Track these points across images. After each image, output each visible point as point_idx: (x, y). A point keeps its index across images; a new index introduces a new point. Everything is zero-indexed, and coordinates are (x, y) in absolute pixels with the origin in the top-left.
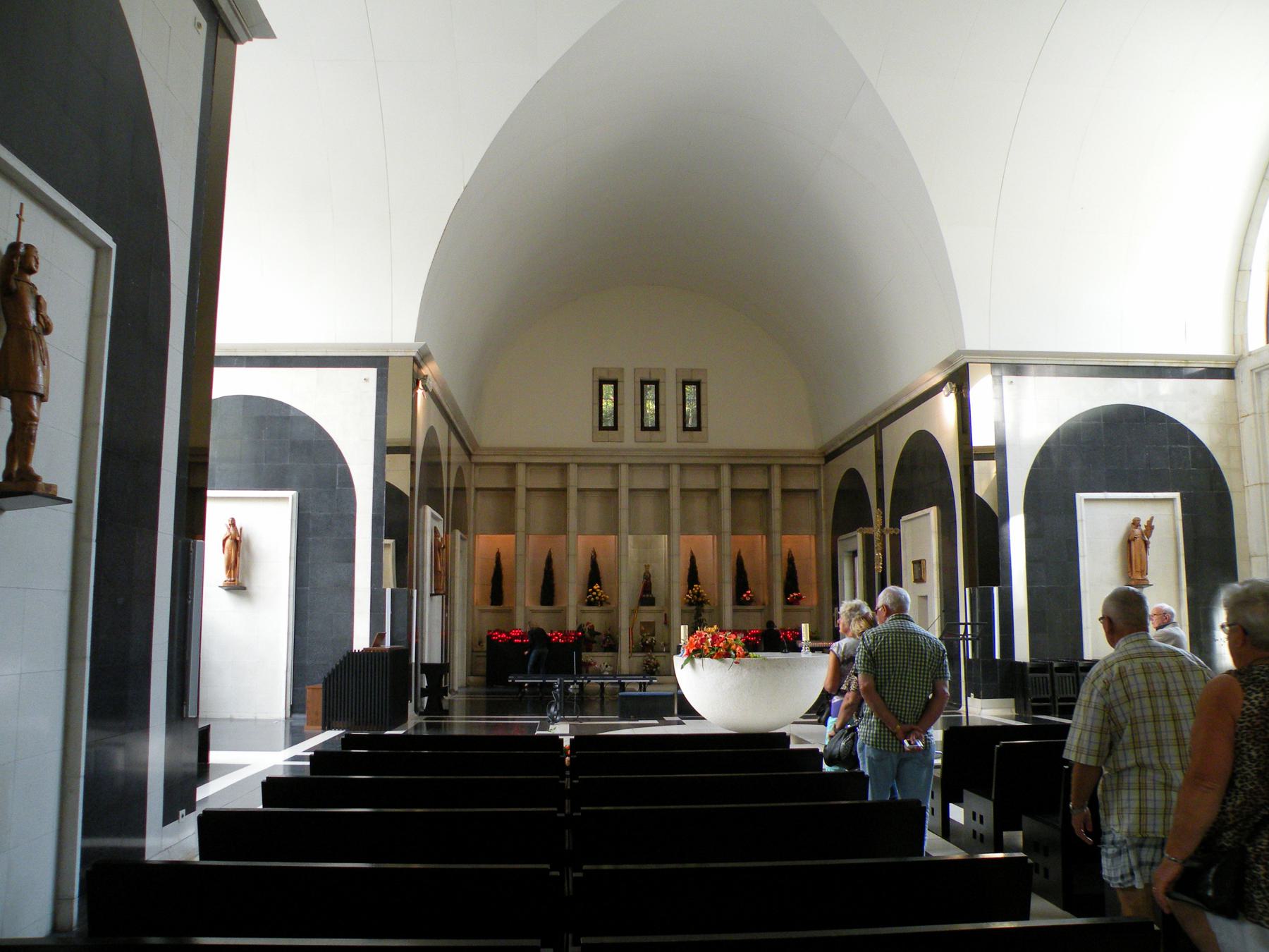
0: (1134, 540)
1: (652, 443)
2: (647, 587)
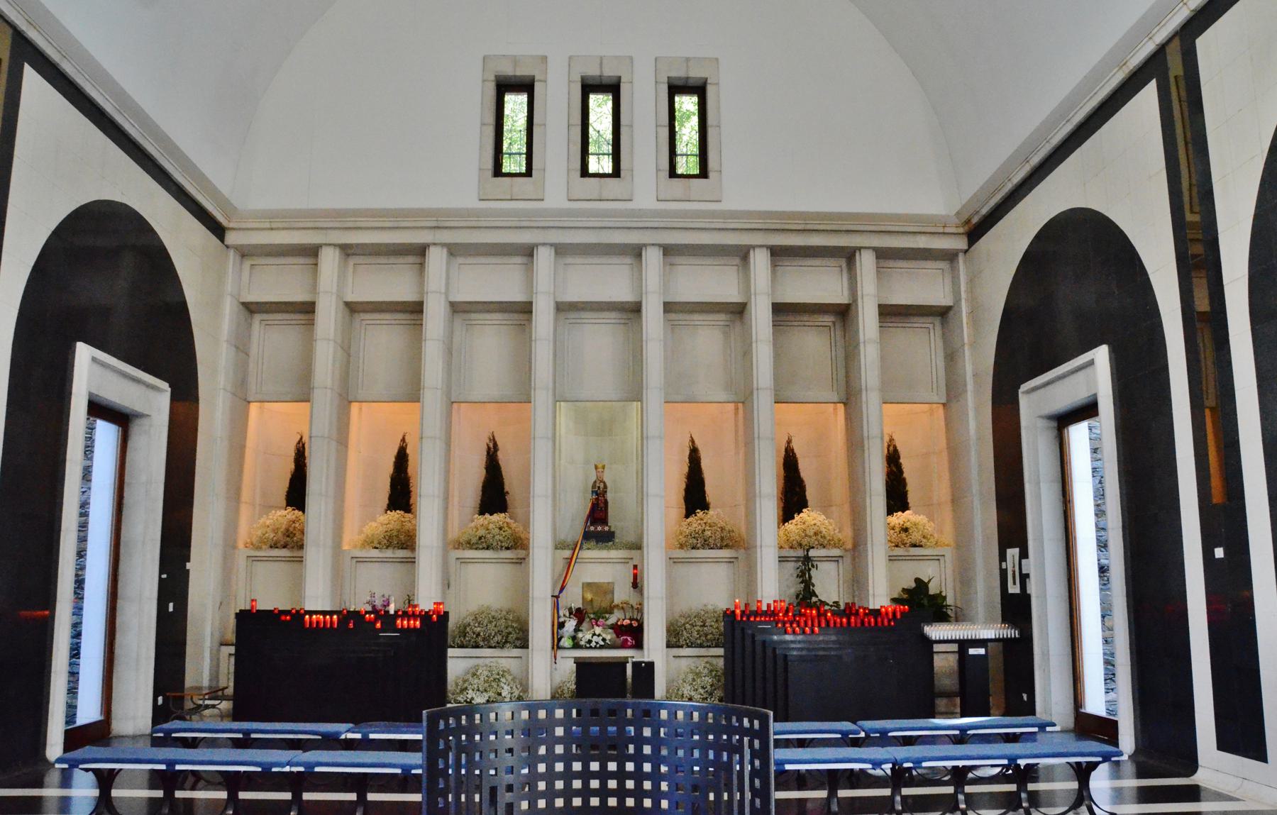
2: (598, 512)
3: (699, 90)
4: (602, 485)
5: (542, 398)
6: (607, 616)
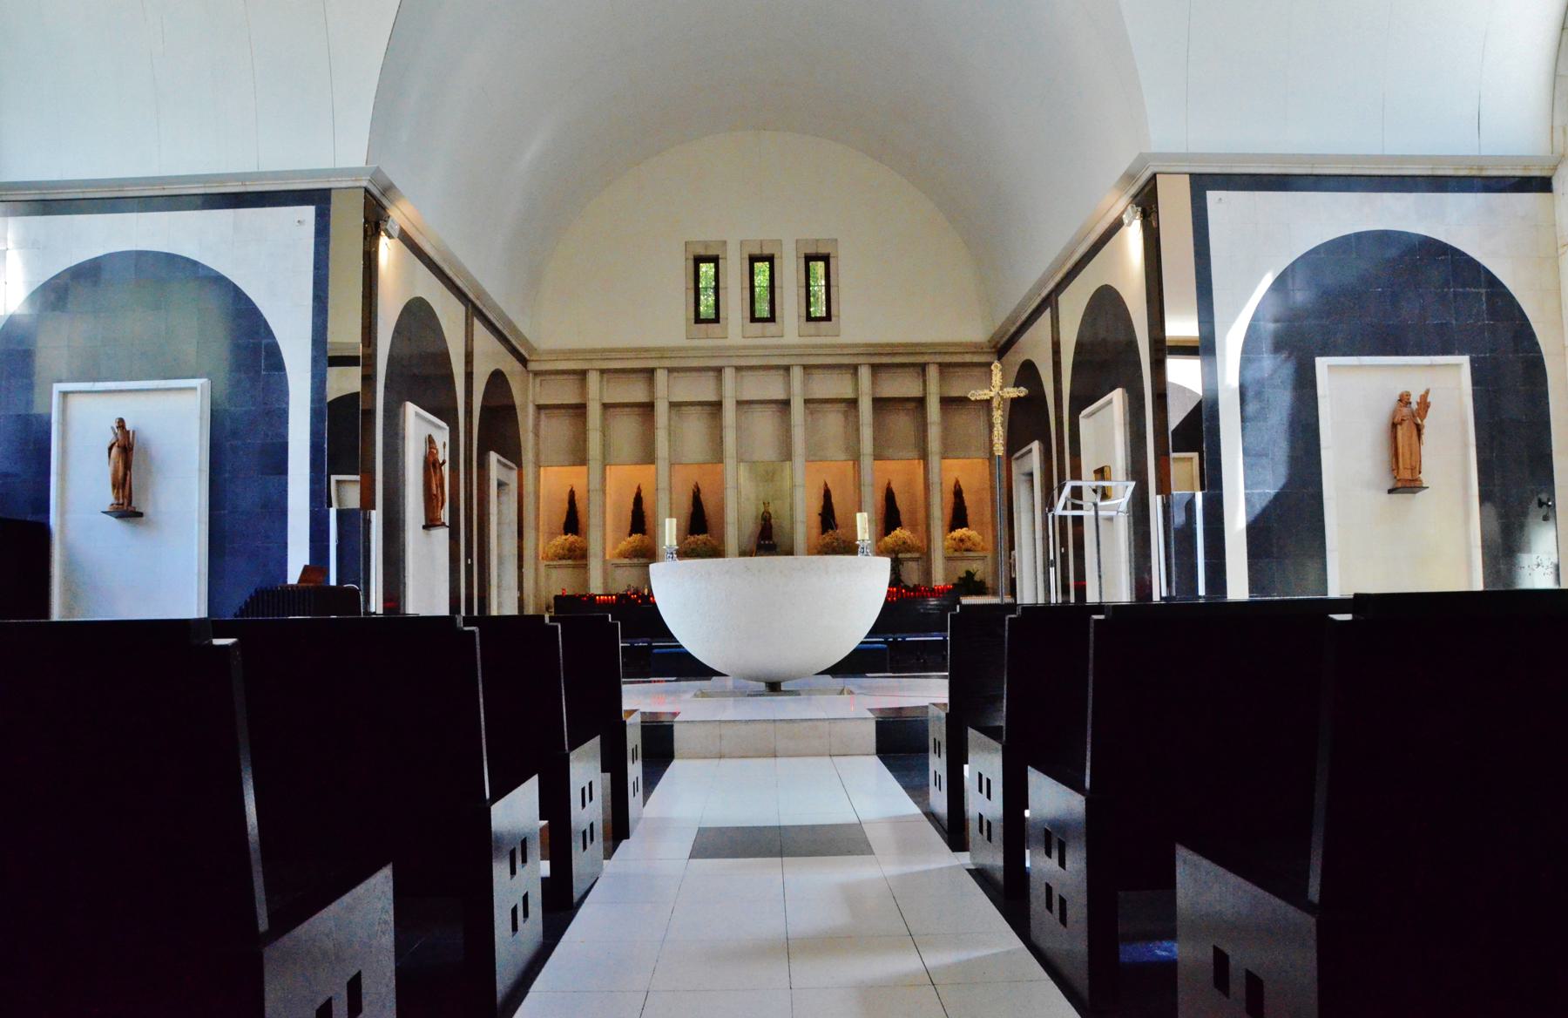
0: (1401, 424)
3: (826, 259)
4: (768, 515)
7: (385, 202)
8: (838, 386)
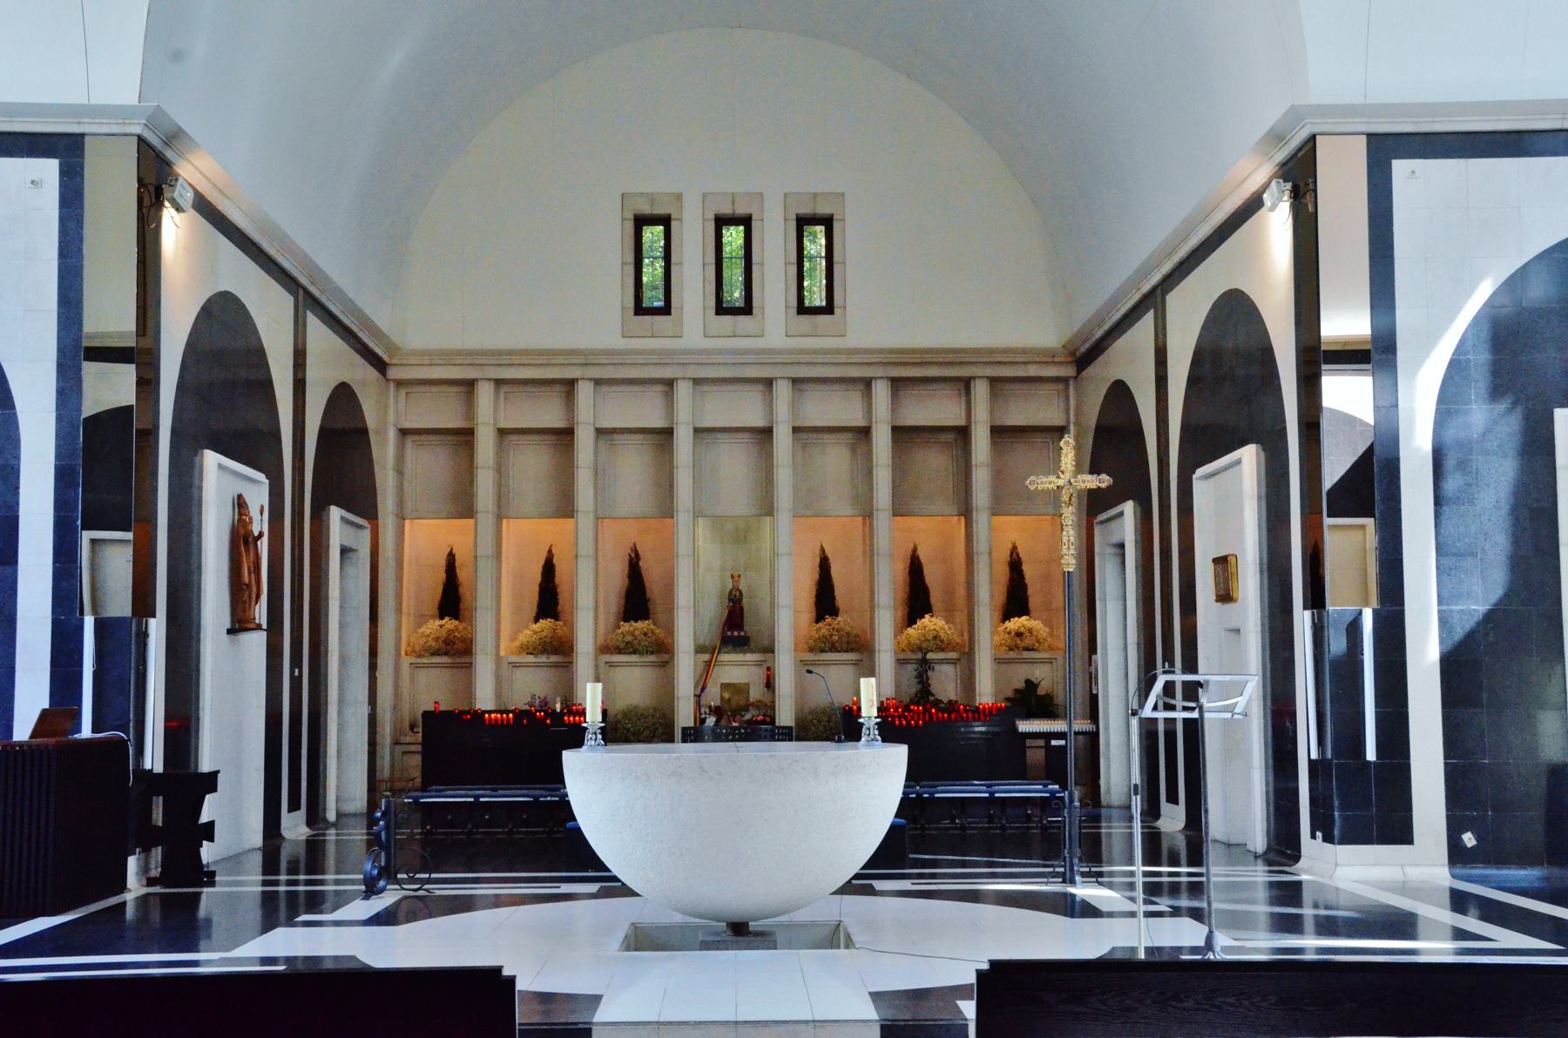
1: (733, 335)
5: (683, 518)
6: (743, 713)
7: (169, 154)
8: (842, 409)
